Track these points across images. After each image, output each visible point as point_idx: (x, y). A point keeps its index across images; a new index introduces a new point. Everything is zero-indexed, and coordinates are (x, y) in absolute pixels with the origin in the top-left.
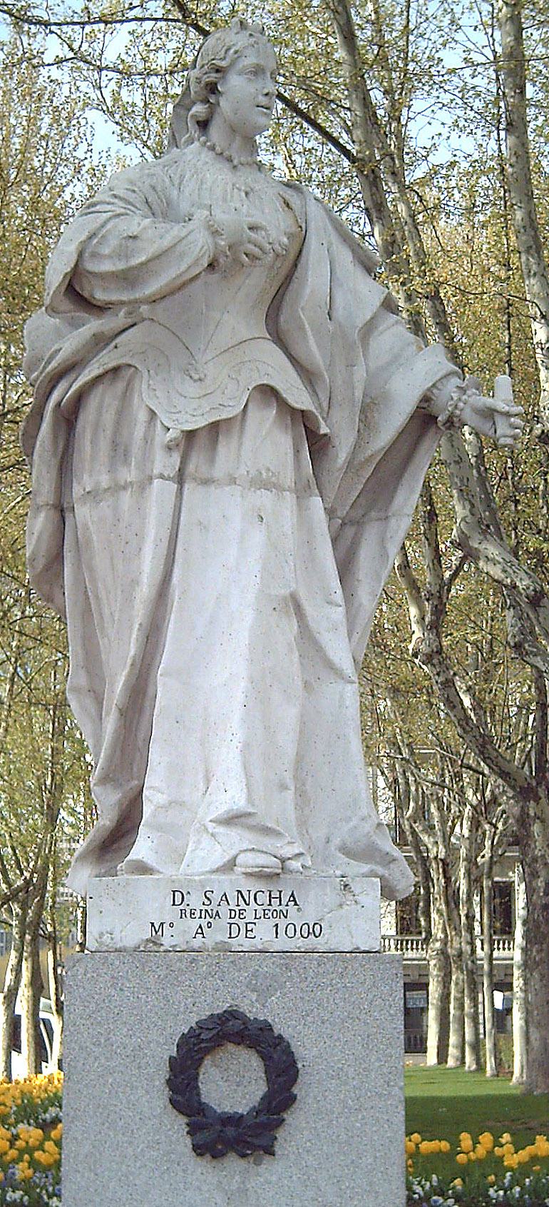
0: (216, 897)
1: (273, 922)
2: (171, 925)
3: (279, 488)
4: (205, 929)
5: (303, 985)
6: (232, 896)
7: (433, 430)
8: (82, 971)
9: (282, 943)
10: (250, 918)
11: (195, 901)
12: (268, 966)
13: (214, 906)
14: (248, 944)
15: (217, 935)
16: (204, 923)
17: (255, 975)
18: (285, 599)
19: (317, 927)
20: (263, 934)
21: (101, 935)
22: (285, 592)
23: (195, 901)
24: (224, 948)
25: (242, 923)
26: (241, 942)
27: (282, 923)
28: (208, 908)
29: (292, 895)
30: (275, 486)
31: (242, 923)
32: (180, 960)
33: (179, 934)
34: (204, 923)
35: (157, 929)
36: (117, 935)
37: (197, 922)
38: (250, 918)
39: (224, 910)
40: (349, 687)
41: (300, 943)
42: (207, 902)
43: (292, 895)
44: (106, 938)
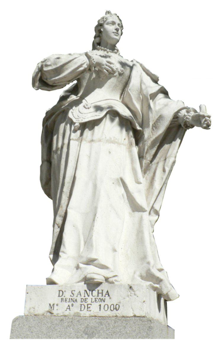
0: (76, 293)
1: (98, 304)
2: (57, 305)
3: (119, 144)
4: (71, 307)
5: (108, 332)
7: (181, 129)
8: (18, 323)
9: (103, 313)
10: (89, 302)
11: (67, 295)
12: (93, 323)
13: (75, 297)
14: (88, 314)
15: (76, 309)
16: (70, 304)
18: (117, 180)
19: (118, 306)
20: (95, 309)
21: (30, 309)
22: (118, 177)
23: (67, 295)
24: (77, 315)
25: (86, 304)
26: (85, 313)
27: (103, 304)
28: (73, 298)
29: (107, 292)
30: (116, 142)
31: (86, 304)
32: (56, 320)
33: (61, 310)
34: (70, 304)
35: (52, 306)
36: (36, 308)
37: (67, 304)
38: (89, 302)
40: (52, 83)
41: (109, 313)
42: (72, 295)
43: (107, 292)
44: (32, 311)
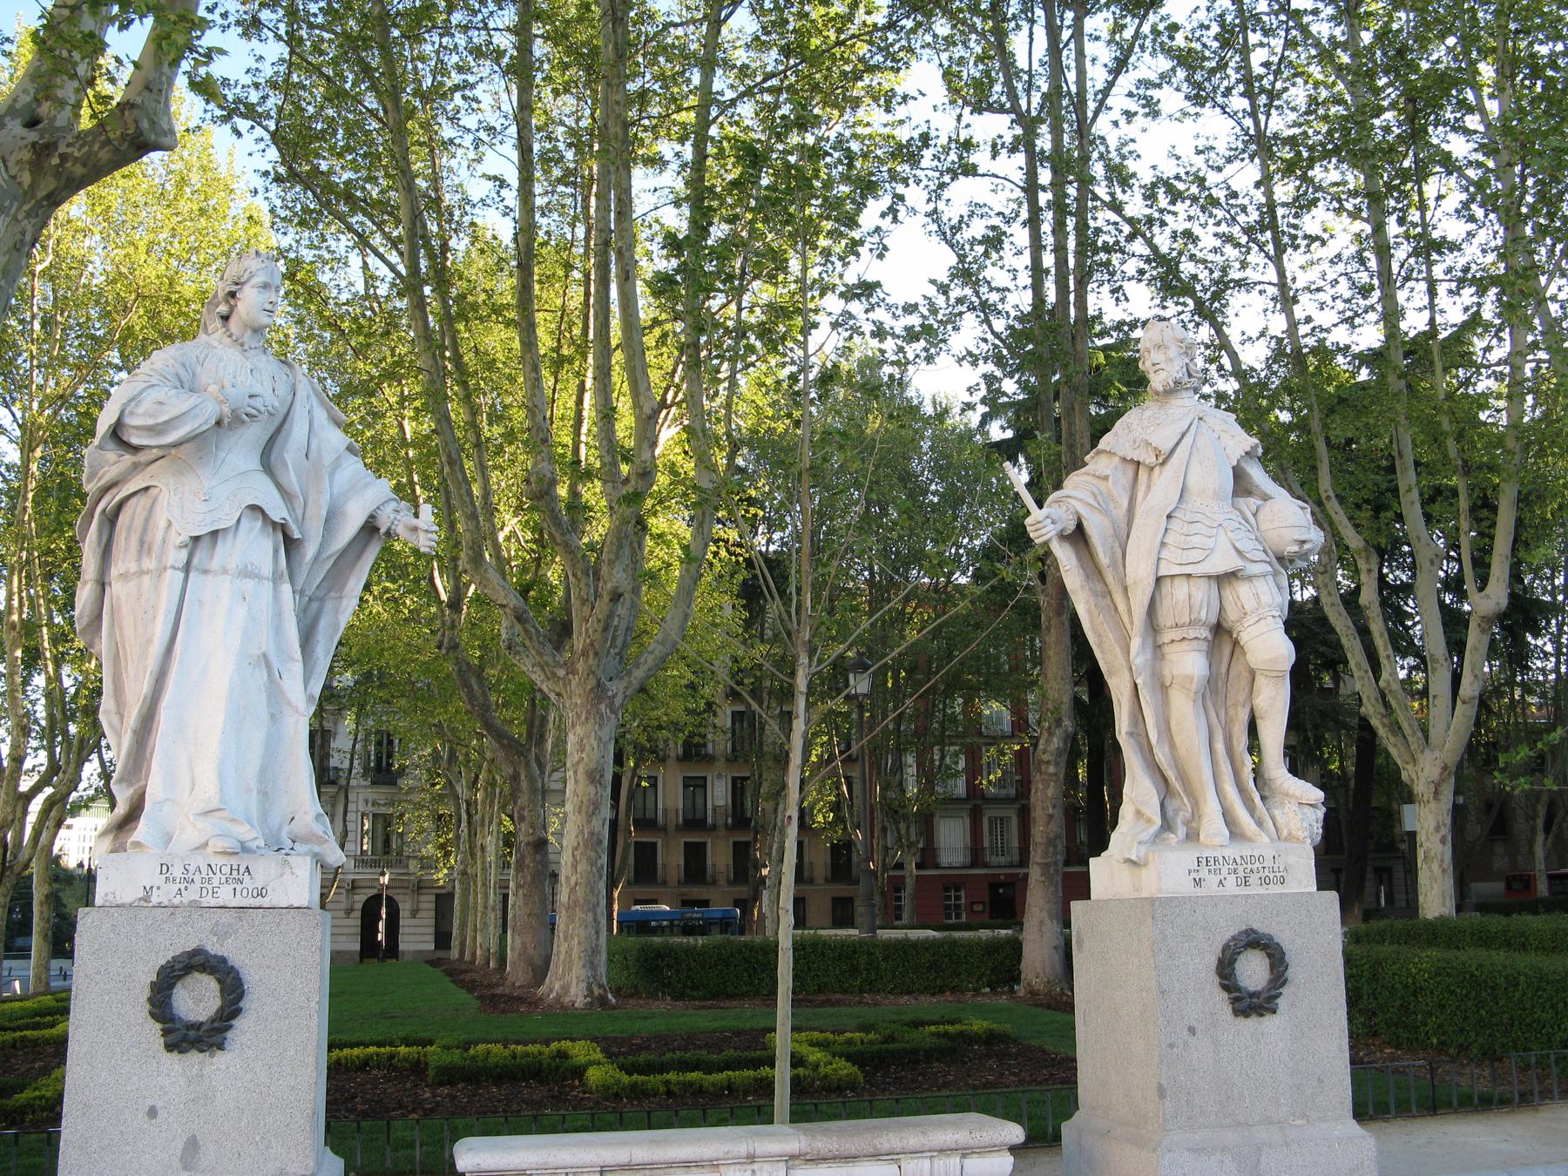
0: (192, 869)
6: (204, 868)
11: (177, 871)
17: (216, 924)
23: (177, 871)
39: (197, 878)
44: (110, 897)
